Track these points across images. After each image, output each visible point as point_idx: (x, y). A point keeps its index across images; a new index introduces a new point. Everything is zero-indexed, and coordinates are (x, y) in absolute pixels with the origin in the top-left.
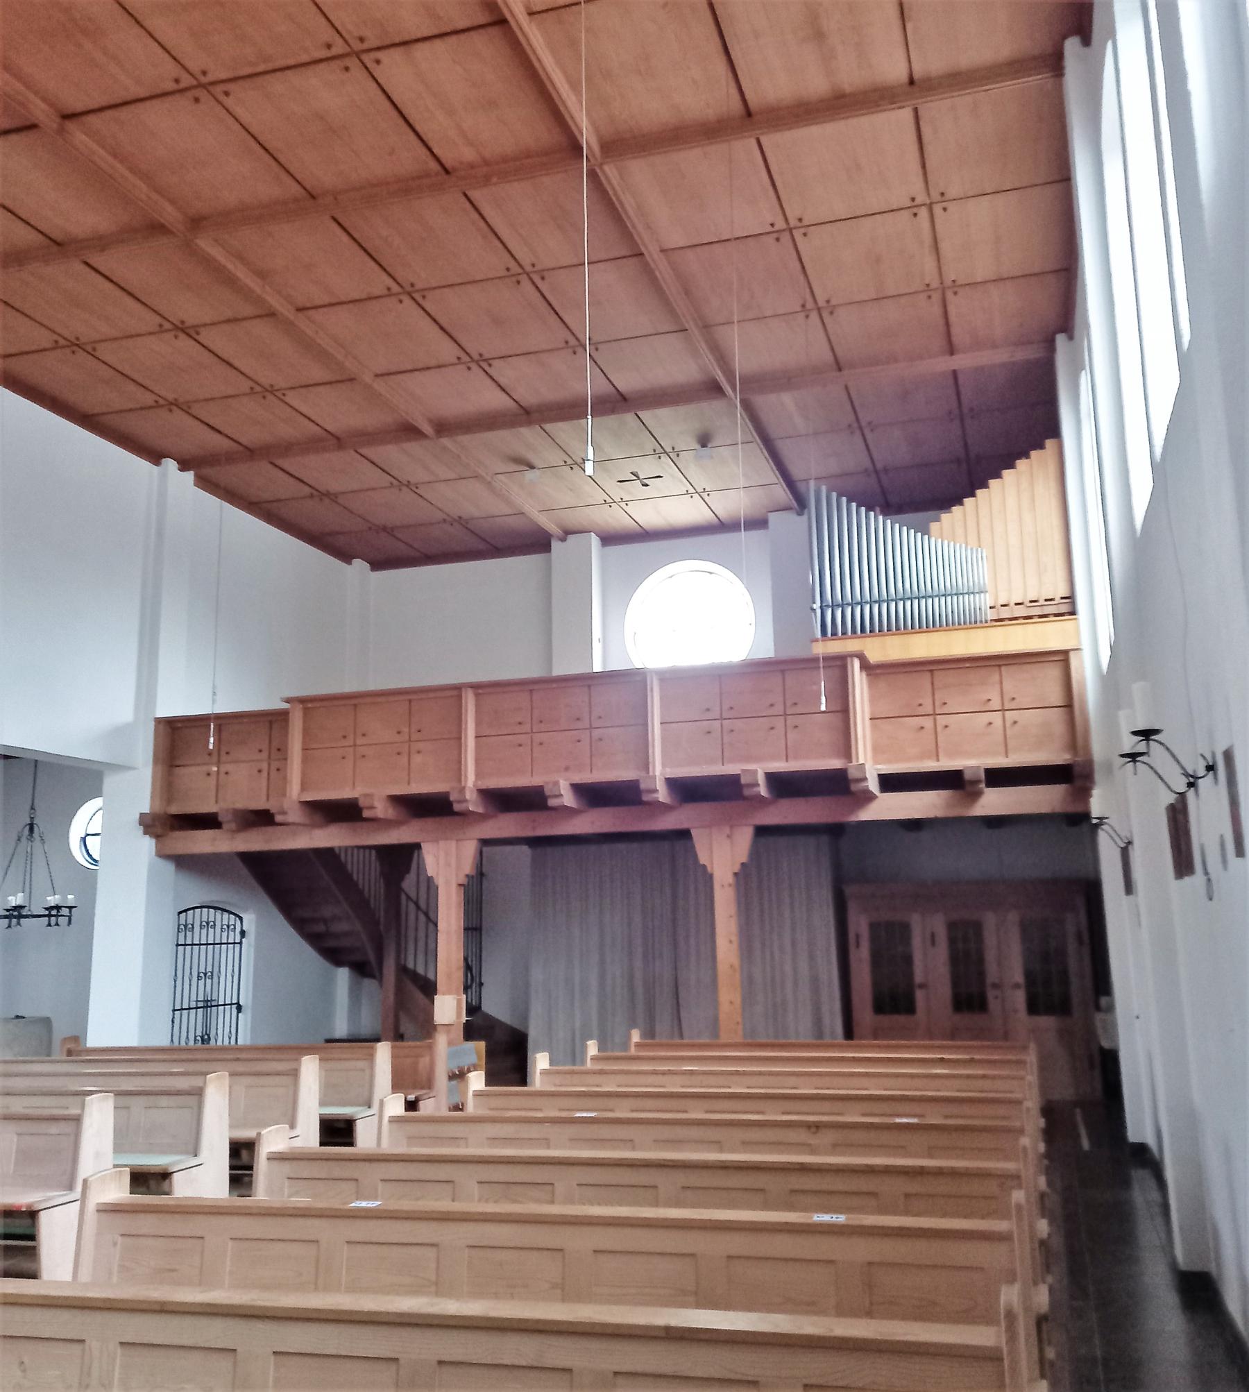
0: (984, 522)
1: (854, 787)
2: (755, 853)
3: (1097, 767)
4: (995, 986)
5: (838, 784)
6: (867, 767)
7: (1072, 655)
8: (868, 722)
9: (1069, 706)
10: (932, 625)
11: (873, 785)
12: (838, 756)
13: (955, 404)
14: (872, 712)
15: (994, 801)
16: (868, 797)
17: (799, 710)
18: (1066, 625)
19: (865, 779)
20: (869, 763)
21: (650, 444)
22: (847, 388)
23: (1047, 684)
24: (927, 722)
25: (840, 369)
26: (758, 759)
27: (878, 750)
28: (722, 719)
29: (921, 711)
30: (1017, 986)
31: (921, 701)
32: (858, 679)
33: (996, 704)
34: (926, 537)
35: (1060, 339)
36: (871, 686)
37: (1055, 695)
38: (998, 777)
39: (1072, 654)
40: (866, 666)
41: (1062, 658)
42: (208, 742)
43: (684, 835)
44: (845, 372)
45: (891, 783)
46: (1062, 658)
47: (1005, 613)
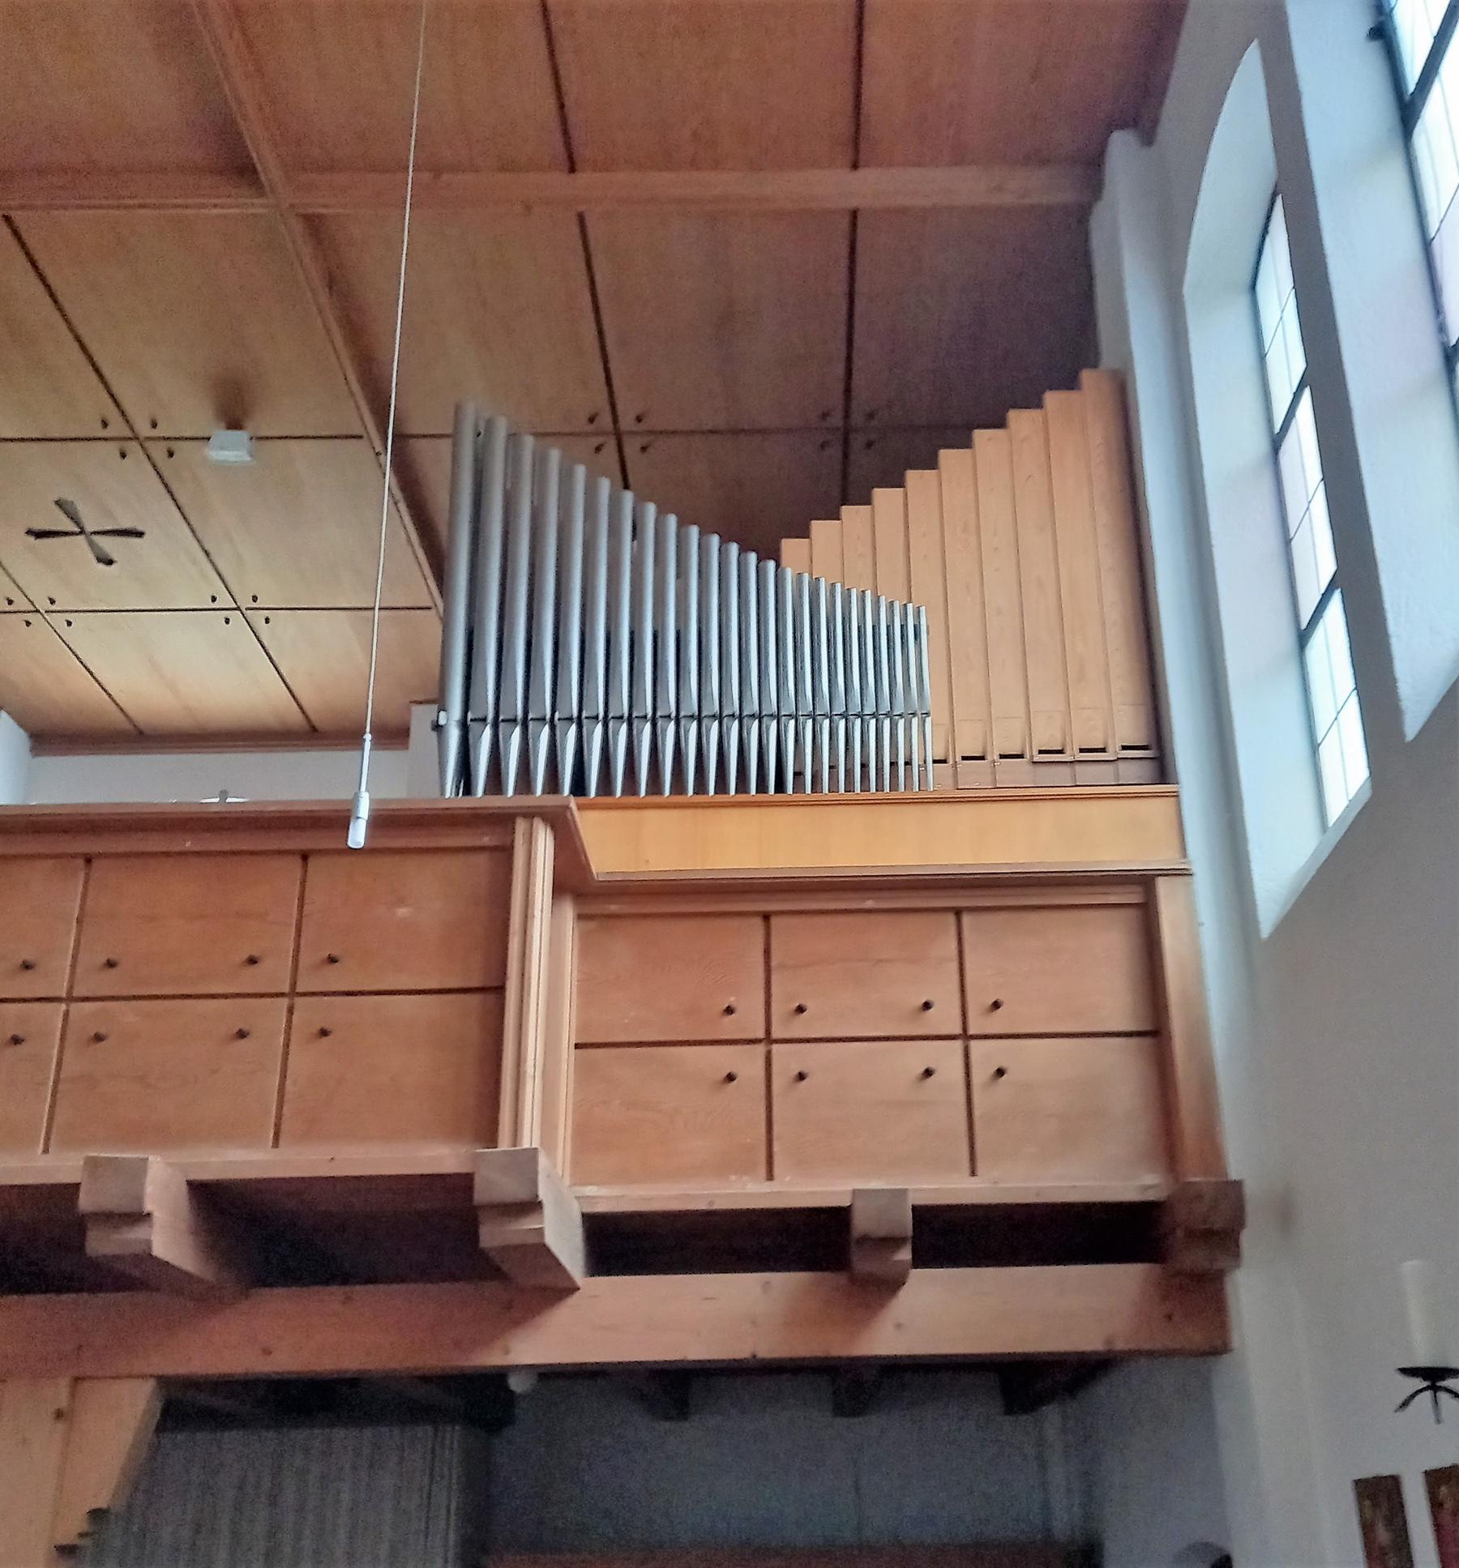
0: (924, 545)
1: (493, 1235)
2: (146, 1477)
3: (1250, 1208)
5: (441, 1235)
6: (543, 1161)
7: (1164, 889)
8: (567, 1055)
9: (1154, 1031)
10: (770, 782)
11: (566, 1244)
12: (452, 1132)
13: (837, 397)
14: (582, 1028)
15: (937, 1312)
16: (536, 1286)
17: (335, 979)
18: (1155, 810)
19: (532, 1206)
20: (562, 1173)
21: (91, 404)
22: (581, 218)
23: (1087, 967)
24: (748, 1062)
25: (572, 170)
26: (162, 1135)
27: (591, 1139)
28: (70, 999)
29: (728, 1028)
31: (731, 1000)
32: (546, 933)
33: (945, 1018)
34: (771, 565)
35: (1122, 147)
36: (587, 949)
37: (1114, 1002)
38: (956, 1236)
39: (1163, 886)
40: (573, 880)
41: (1137, 895)
44: (583, 178)
45: (620, 1244)
46: (1137, 895)
47: (975, 777)
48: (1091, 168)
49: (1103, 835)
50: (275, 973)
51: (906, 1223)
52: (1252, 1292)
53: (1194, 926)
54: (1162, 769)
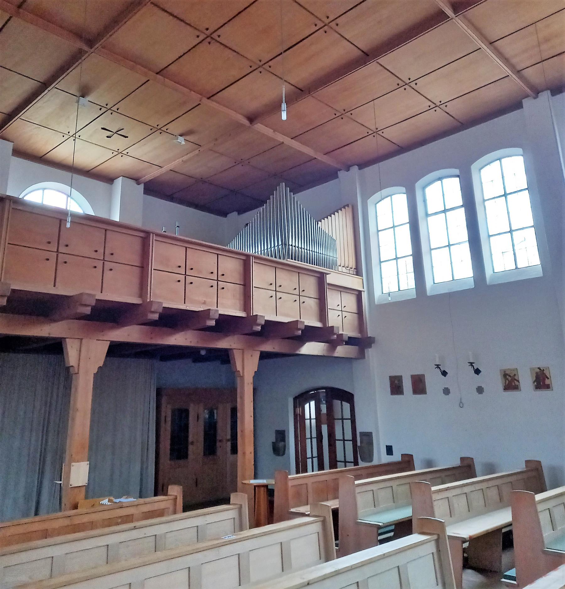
4: (220, 441)
15: (341, 351)
30: (228, 440)
35: (355, 169)
41: (359, 295)
42: (59, 217)
43: (55, 347)
48: (348, 169)
49: (354, 282)
50: (340, 313)
51: (347, 339)
52: (370, 353)
53: (365, 296)
54: (358, 272)
